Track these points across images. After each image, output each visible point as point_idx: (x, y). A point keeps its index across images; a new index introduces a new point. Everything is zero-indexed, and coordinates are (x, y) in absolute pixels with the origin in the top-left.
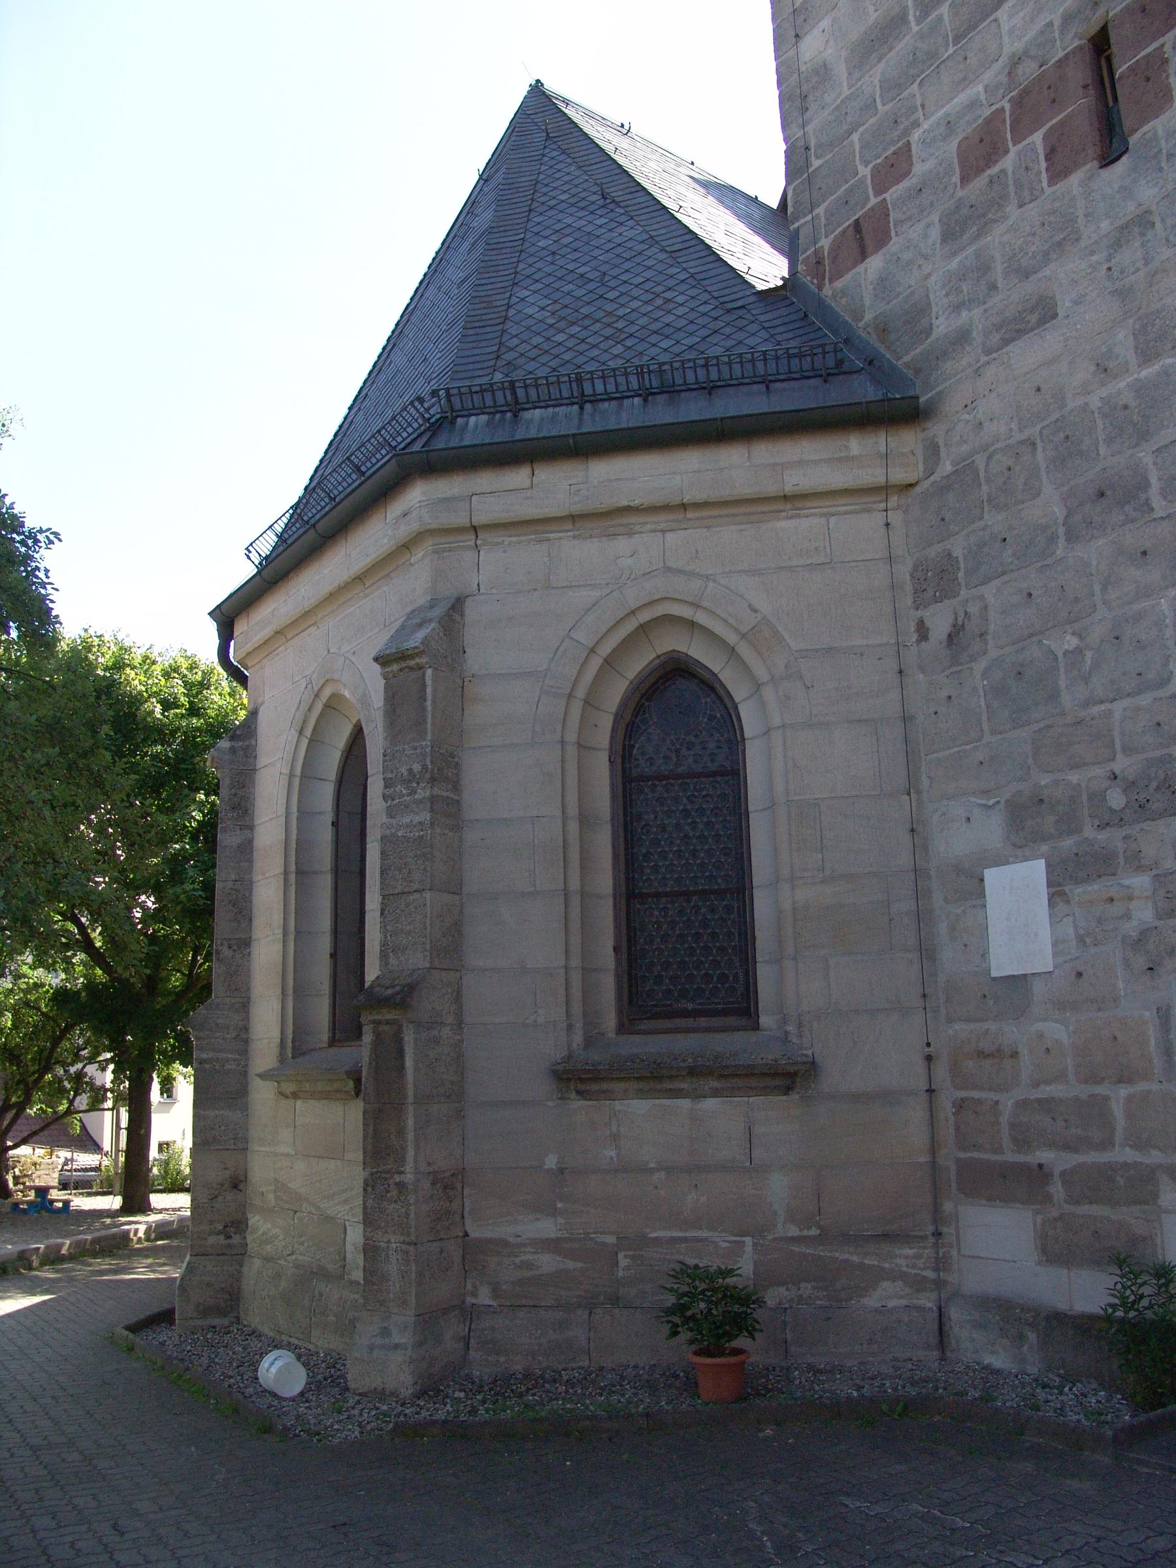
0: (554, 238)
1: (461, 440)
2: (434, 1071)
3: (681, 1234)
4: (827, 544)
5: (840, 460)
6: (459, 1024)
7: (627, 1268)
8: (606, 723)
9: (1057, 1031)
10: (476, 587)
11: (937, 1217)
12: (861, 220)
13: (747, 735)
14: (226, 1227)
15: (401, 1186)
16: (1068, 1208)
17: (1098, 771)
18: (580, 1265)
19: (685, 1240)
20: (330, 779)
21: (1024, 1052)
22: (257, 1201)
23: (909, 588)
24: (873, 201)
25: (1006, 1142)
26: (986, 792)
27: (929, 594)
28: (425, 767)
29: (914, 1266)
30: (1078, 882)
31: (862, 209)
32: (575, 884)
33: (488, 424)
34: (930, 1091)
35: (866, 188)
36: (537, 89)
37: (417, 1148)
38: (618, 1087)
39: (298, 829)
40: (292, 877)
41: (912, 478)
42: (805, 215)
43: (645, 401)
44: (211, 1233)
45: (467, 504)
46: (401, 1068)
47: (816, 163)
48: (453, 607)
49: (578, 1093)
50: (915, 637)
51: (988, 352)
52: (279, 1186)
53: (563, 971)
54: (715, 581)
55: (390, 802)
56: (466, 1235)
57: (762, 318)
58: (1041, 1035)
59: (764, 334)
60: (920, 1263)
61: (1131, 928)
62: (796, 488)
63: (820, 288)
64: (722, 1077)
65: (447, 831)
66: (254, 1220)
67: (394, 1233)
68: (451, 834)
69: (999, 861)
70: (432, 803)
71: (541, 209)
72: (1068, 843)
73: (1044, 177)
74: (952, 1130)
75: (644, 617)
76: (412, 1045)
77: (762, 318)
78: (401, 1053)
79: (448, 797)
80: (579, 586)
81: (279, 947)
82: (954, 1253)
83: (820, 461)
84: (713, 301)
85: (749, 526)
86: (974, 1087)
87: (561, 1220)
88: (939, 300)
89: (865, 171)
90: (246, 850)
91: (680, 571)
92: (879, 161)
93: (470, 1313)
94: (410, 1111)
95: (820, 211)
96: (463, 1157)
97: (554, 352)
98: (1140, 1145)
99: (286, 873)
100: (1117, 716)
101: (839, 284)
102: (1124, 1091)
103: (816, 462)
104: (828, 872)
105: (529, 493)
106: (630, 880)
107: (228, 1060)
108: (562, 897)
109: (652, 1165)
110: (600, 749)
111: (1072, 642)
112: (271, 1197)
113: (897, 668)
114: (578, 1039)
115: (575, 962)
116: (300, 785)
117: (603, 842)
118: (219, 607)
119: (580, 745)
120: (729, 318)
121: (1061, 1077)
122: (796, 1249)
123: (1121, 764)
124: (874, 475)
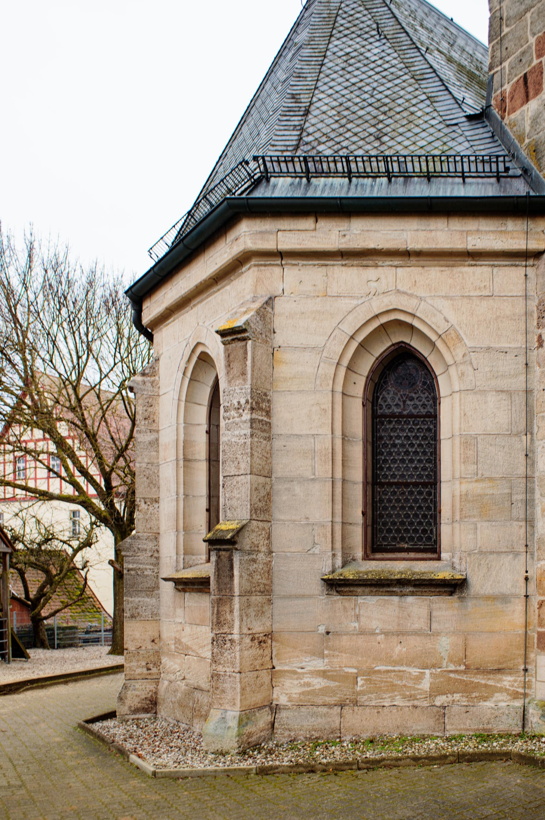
0: (345, 58)
1: (273, 193)
2: (252, 578)
3: (392, 668)
4: (491, 284)
7: (362, 686)
8: (361, 382)
10: (281, 291)
12: (528, 75)
13: (441, 395)
14: (147, 664)
18: (337, 683)
19: (394, 671)
20: (359, 395)
22: (165, 649)
23: (535, 316)
24: (535, 62)
28: (247, 402)
29: (513, 686)
31: (529, 66)
32: (339, 475)
33: (292, 184)
34: (527, 596)
35: (532, 53)
38: (359, 590)
39: (185, 434)
40: (181, 463)
42: (497, 66)
43: (390, 180)
44: (138, 667)
45: (275, 237)
46: (232, 576)
47: (506, 30)
48: (267, 303)
49: (337, 592)
50: (536, 344)
52: (178, 641)
53: (330, 524)
54: (425, 301)
55: (227, 420)
56: (274, 668)
57: (467, 133)
59: (466, 144)
60: (516, 684)
62: (474, 247)
63: (503, 118)
64: (415, 586)
65: (262, 440)
66: (164, 660)
67: (228, 667)
68: (265, 442)
70: (251, 423)
71: (338, 35)
74: (537, 617)
75: (384, 319)
76: (238, 563)
77: (467, 133)
78: (232, 568)
79: (262, 420)
80: (344, 297)
82: (534, 680)
83: (490, 231)
84: (439, 118)
85: (447, 268)
87: (326, 660)
89: (532, 40)
91: (405, 293)
92: (540, 34)
93: (275, 709)
94: (236, 600)
95: (506, 64)
96: (272, 625)
97: (337, 139)
99: (177, 460)
101: (513, 116)
104: (479, 476)
105: (313, 234)
106: (375, 476)
107: (146, 569)
108: (331, 483)
109: (377, 631)
110: (357, 397)
113: (525, 362)
114: (339, 562)
115: (338, 519)
116: (185, 407)
118: (131, 288)
119: (343, 394)
120: (446, 130)
122: (452, 675)
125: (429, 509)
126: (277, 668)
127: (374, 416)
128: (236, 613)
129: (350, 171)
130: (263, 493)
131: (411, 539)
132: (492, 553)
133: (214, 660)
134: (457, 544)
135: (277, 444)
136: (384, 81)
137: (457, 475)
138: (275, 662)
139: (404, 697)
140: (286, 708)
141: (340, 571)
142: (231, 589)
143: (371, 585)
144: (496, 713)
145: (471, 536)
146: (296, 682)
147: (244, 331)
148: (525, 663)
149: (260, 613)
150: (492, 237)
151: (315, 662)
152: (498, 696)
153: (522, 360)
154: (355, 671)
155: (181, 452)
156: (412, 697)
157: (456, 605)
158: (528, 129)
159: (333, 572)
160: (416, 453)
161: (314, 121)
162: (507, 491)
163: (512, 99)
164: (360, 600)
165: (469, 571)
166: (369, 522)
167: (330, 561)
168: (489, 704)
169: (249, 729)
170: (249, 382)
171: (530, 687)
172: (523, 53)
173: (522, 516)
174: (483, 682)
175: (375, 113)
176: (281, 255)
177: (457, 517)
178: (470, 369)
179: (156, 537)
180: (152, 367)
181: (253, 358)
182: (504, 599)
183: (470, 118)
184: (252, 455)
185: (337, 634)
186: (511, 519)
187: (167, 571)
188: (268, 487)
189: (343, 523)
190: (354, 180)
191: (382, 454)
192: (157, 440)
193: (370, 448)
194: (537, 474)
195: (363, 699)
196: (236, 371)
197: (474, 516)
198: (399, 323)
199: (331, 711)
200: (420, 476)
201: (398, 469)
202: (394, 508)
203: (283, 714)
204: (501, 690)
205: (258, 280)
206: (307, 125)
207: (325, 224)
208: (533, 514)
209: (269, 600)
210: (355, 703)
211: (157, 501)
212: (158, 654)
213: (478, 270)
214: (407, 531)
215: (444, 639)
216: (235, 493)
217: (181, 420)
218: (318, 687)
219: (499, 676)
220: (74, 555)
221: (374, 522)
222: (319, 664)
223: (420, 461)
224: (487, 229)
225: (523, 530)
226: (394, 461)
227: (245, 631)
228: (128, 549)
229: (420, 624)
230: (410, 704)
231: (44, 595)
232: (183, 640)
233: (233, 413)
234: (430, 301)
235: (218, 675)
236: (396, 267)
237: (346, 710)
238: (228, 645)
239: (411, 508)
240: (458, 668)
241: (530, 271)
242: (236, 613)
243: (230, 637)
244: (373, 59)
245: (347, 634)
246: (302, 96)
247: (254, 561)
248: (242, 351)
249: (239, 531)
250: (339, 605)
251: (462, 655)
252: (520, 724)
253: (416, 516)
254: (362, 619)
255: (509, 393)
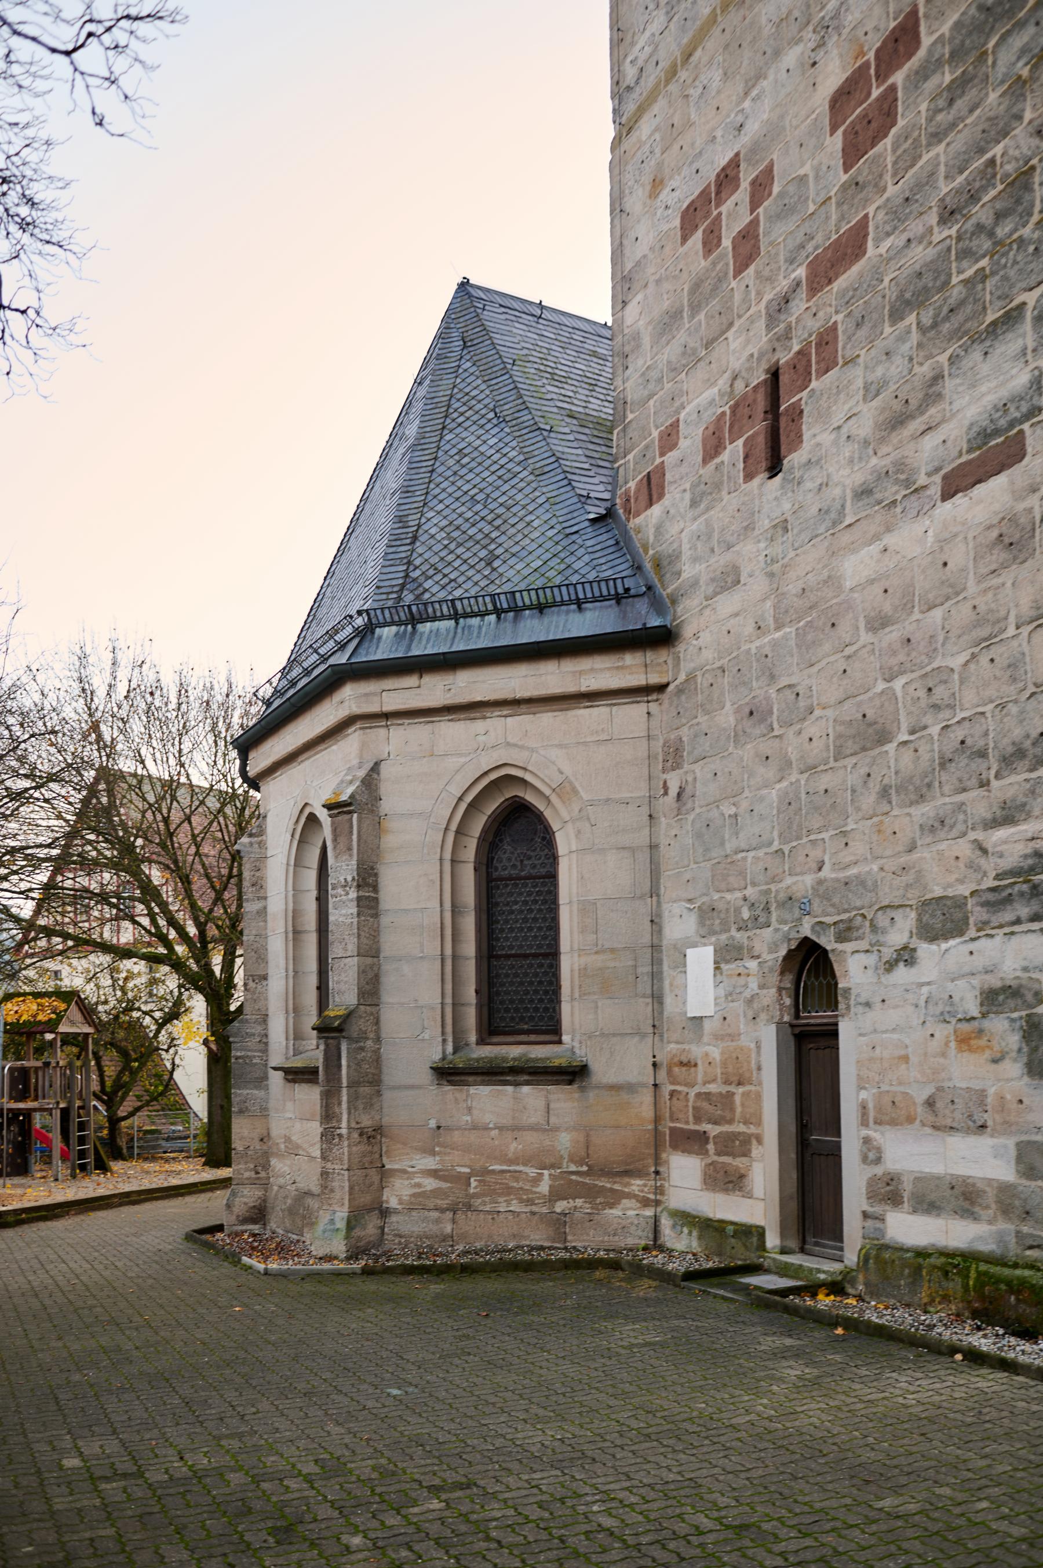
0: (457, 457)
5: (618, 668)
6: (378, 1040)
9: (715, 1053)
11: (658, 1161)
15: (340, 1136)
16: (716, 1158)
17: (738, 895)
21: (700, 1063)
23: (661, 759)
24: (658, 461)
25: (691, 1119)
26: (690, 901)
27: (669, 764)
30: (727, 962)
32: (448, 952)
33: (397, 634)
34: (655, 1085)
36: (464, 286)
37: (349, 1113)
38: (471, 1079)
40: (290, 935)
41: (664, 680)
43: (499, 618)
44: (246, 1170)
46: (340, 1066)
47: (630, 416)
51: (707, 599)
52: (288, 1139)
58: (707, 1055)
61: (747, 994)
64: (530, 1074)
66: (274, 1161)
69: (694, 945)
72: (723, 937)
73: (741, 474)
77: (589, 543)
81: (283, 982)
86: (679, 1084)
87: (438, 1158)
88: (686, 554)
89: (655, 434)
90: (263, 912)
91: (515, 745)
93: (384, 1213)
94: (344, 1091)
95: (630, 457)
98: (746, 1123)
99: (286, 932)
100: (749, 860)
102: (741, 1090)
103: (602, 670)
105: (418, 691)
106: (491, 948)
111: (733, 810)
112: (282, 1146)
114: (450, 1048)
115: (449, 1000)
117: (469, 924)
121: (714, 1080)
122: (574, 1177)
123: (750, 892)
124: (637, 680)
125: (551, 983)
126: (387, 1167)
127: (490, 879)
128: (344, 1106)
129: (456, 613)
130: (370, 975)
131: (532, 1018)
132: (614, 1035)
133: (324, 1158)
134: (577, 1027)
135: (385, 920)
136: (500, 482)
137: (576, 947)
138: (385, 1160)
139: (521, 1201)
140: (396, 1212)
141: (451, 1057)
142: (339, 1080)
143: (483, 1074)
144: (624, 1223)
145: (591, 1016)
146: (406, 1182)
147: (350, 804)
148: (656, 1164)
149: (369, 1106)
150: (608, 674)
151: (425, 1161)
152: (626, 1202)
153: (645, 811)
154: (468, 1170)
155: (290, 923)
156: (530, 1202)
157: (576, 1095)
158: (651, 539)
159: (444, 1059)
160: (535, 919)
161: (420, 550)
162: (630, 963)
163: (636, 499)
164: (472, 1090)
165: (590, 1057)
166: (485, 1000)
167: (440, 1048)
168: (616, 1212)
169: (357, 1232)
170: (355, 858)
171: (662, 1193)
172: (647, 447)
173: (649, 992)
174: (608, 1185)
175: (487, 529)
176: (387, 716)
177: (577, 995)
178: (588, 825)
179: (264, 1019)
180: (260, 826)
181: (359, 832)
182: (630, 1088)
183: (593, 521)
184: (359, 935)
185: (449, 1129)
186: (636, 995)
187: (276, 1059)
188: (375, 968)
189: (454, 1004)
190: (461, 620)
191: (498, 922)
192: (265, 908)
193: (484, 917)
194: (665, 943)
195: (477, 1202)
196: (342, 846)
197: (594, 993)
198: (509, 779)
199: (443, 1216)
200: (540, 946)
201: (516, 939)
202: (512, 983)
203: (394, 1218)
204: (629, 1196)
205: (364, 745)
206: (415, 555)
207: (429, 680)
208: (661, 989)
209: (379, 1091)
210: (469, 1207)
211: (265, 978)
212: (266, 1155)
213: (595, 711)
214: (527, 1009)
215: (564, 1134)
216: (343, 977)
217: (290, 888)
218: (429, 1188)
219: (626, 1180)
220: (158, 1032)
221: (490, 1000)
222: (430, 1163)
223: (540, 929)
224: (603, 666)
225: (650, 1008)
226: (512, 930)
227: (353, 1125)
228: (236, 1035)
229: (535, 1117)
230: (527, 1209)
231: (122, 1086)
232: (294, 1138)
233: (340, 891)
234: (542, 752)
235: (327, 1173)
236: (506, 716)
237: (460, 1215)
238: (337, 1140)
239: (531, 983)
240: (580, 1169)
241: (653, 707)
242: (344, 1106)
243: (338, 1131)
244: (489, 453)
245: (458, 1128)
246: (410, 518)
247: (362, 1049)
248: (347, 825)
249: (349, 1016)
250: (450, 1096)
251: (583, 1154)
252: (651, 1236)
253: (536, 992)
254: (475, 1112)
255: (632, 850)
